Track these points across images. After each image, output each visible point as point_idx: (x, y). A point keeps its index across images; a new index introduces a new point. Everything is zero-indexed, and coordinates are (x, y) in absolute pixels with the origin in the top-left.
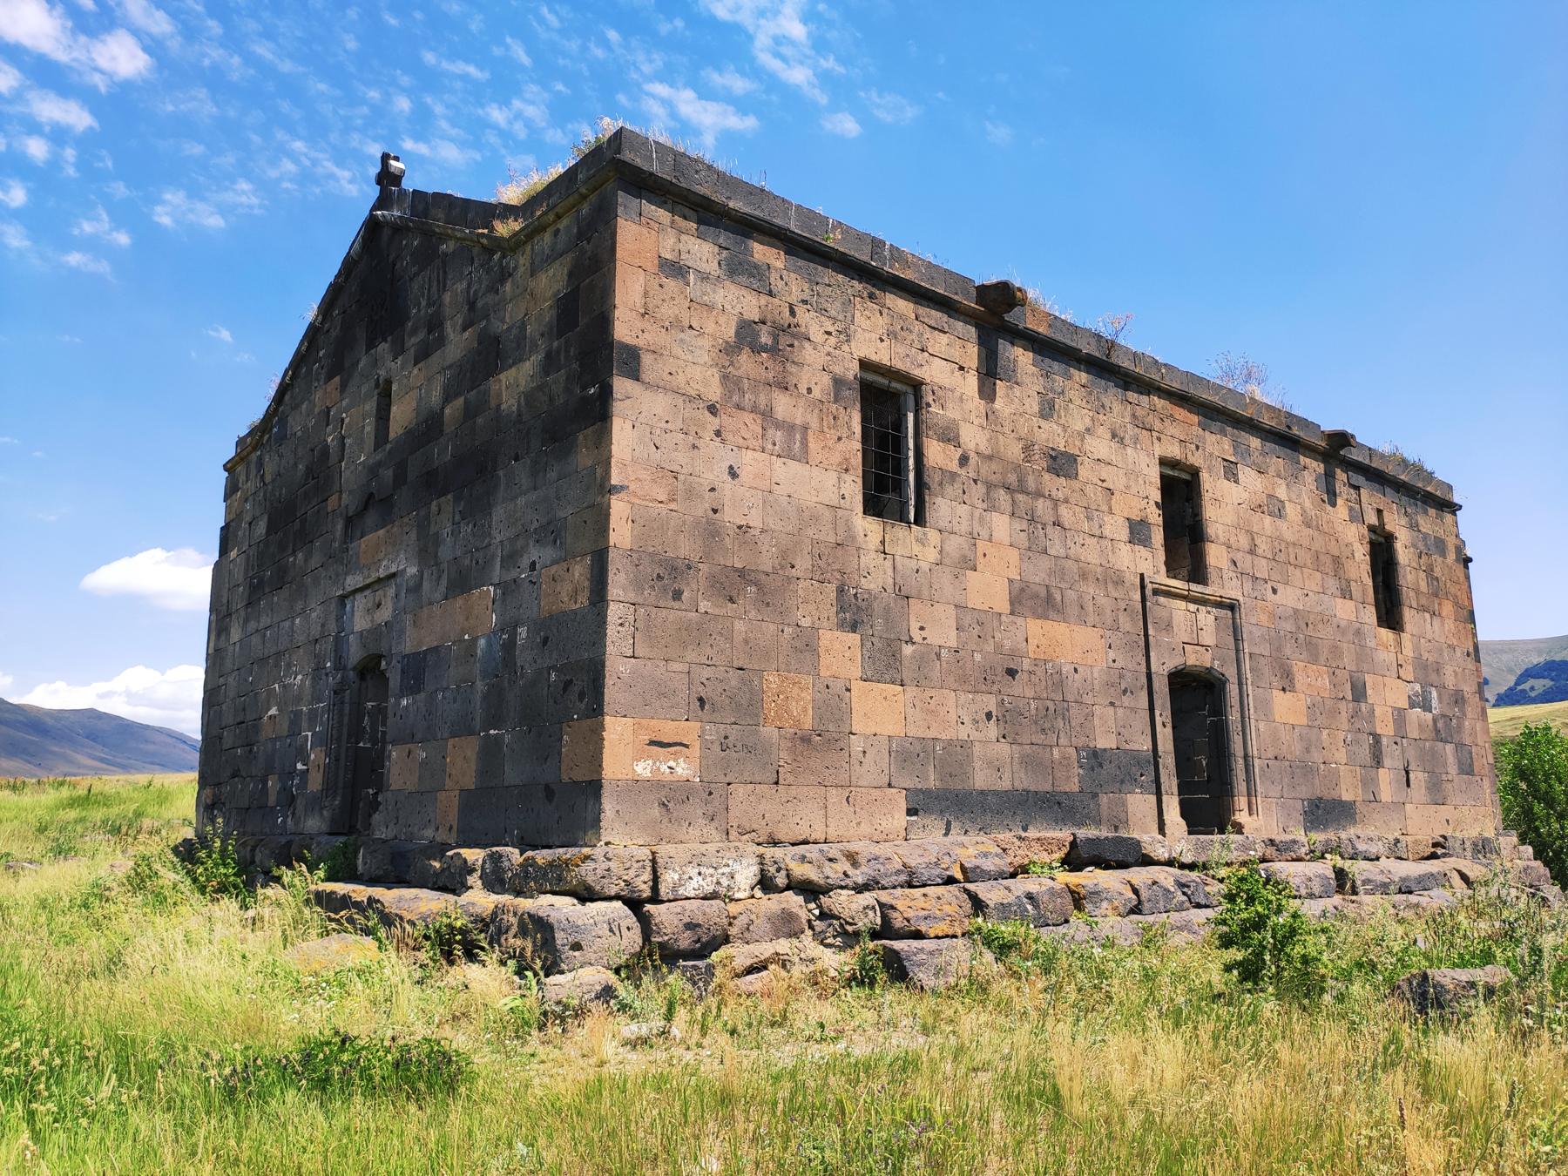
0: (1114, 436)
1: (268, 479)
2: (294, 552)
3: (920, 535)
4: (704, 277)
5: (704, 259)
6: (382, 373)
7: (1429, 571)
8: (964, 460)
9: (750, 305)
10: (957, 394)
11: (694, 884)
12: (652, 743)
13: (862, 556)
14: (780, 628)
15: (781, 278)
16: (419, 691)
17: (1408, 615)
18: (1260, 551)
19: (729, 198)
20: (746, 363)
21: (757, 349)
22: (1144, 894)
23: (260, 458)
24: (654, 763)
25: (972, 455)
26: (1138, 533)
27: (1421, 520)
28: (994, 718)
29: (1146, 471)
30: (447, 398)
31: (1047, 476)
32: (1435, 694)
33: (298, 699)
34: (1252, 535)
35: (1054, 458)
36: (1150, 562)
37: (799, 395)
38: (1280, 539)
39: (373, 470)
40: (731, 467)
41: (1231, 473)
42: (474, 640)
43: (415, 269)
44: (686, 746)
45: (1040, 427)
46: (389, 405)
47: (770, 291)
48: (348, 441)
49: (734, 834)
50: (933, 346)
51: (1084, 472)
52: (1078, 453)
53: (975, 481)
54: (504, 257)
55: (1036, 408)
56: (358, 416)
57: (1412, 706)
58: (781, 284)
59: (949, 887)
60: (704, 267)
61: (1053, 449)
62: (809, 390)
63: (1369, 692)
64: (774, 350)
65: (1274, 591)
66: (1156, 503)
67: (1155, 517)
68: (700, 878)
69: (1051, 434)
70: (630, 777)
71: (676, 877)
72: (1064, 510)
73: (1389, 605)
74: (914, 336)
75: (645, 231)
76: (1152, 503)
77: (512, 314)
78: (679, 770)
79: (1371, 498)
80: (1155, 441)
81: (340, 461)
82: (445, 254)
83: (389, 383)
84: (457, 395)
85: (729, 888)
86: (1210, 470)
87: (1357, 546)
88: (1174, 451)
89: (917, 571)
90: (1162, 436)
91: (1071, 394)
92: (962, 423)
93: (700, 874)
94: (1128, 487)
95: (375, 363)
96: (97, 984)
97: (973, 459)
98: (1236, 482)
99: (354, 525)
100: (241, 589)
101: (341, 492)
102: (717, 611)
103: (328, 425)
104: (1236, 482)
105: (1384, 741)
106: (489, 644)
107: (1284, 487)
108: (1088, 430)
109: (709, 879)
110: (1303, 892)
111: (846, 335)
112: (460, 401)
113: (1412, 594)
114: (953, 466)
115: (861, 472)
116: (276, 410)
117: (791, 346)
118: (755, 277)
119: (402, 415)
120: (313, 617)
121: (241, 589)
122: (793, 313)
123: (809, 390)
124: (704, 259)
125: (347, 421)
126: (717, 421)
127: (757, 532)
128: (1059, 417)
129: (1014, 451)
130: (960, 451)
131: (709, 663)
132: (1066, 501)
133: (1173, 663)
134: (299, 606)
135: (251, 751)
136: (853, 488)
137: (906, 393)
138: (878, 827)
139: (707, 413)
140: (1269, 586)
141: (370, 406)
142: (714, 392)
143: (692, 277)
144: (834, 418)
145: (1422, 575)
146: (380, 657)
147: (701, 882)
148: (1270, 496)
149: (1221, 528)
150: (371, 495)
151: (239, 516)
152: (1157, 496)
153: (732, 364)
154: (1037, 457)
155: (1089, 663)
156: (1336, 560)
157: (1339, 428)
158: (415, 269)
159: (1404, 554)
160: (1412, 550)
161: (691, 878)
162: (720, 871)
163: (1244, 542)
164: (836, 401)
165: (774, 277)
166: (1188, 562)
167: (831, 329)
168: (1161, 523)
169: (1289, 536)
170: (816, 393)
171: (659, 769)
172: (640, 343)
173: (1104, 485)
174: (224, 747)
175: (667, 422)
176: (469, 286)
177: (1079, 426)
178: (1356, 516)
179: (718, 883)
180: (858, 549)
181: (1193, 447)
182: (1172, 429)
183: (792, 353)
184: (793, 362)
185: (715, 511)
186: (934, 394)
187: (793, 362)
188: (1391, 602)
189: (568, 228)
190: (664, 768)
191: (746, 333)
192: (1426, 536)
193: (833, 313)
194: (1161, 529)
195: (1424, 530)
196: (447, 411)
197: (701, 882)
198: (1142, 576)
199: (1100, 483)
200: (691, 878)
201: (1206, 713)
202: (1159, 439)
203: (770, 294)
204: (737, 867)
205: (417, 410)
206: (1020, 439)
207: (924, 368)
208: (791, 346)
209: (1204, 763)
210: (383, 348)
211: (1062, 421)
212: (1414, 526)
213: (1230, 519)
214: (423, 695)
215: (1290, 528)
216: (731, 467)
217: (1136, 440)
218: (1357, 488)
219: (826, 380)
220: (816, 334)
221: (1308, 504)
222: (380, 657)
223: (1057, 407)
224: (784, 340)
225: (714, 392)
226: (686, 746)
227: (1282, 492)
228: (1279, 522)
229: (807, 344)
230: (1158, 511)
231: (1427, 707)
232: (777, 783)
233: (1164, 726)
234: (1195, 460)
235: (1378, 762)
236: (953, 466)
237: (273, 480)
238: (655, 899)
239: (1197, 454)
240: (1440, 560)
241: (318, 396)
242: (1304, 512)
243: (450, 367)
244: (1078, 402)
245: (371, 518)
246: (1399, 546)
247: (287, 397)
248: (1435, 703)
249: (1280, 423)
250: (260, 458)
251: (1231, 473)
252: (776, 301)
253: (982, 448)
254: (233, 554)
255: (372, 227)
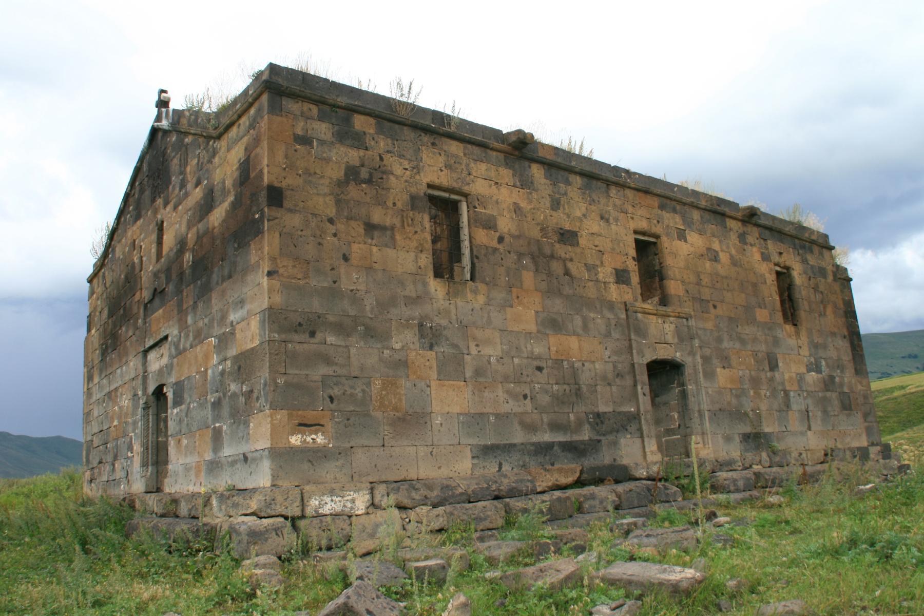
0: (602, 218)
1: (108, 285)
2: (121, 327)
3: (473, 288)
4: (322, 142)
5: (323, 132)
6: (159, 217)
7: (816, 289)
8: (501, 240)
9: (353, 156)
10: (494, 198)
11: (328, 506)
12: (300, 425)
13: (434, 303)
14: (381, 351)
15: (373, 139)
16: (181, 405)
17: (802, 314)
18: (704, 283)
19: (338, 96)
20: (353, 192)
21: (359, 181)
22: (623, 497)
23: (104, 273)
24: (302, 437)
25: (506, 236)
26: (621, 277)
27: (809, 257)
28: (529, 398)
29: (625, 238)
30: (189, 228)
31: (557, 246)
32: (823, 363)
33: (127, 414)
34: (698, 275)
35: (562, 234)
36: (630, 293)
37: (387, 208)
38: (717, 274)
39: (156, 275)
40: (344, 255)
41: (682, 236)
42: (206, 370)
43: (173, 154)
44: (322, 426)
45: (551, 216)
46: (163, 235)
47: (366, 147)
48: (144, 259)
49: (356, 478)
50: (476, 171)
51: (583, 241)
52: (578, 230)
53: (509, 252)
54: (214, 142)
55: (548, 205)
56: (148, 244)
57: (809, 371)
58: (373, 143)
59: (495, 502)
60: (323, 137)
61: (561, 229)
62: (394, 204)
63: (780, 364)
64: (369, 181)
65: (715, 307)
66: (633, 258)
67: (632, 266)
68: (333, 504)
69: (560, 219)
70: (287, 445)
71: (317, 503)
72: (569, 265)
73: (792, 311)
74: (463, 167)
75: (285, 119)
76: (630, 257)
77: (217, 176)
78: (319, 440)
79: (772, 247)
80: (630, 220)
81: (141, 271)
82: (188, 144)
83: (162, 222)
84: (194, 226)
85: (352, 508)
86: (668, 235)
87: (767, 275)
88: (643, 225)
89: (472, 310)
90: (634, 216)
91: (571, 194)
92: (498, 217)
93: (332, 500)
94: (613, 249)
95: (156, 212)
96: (380, 600)
97: (508, 239)
98: (686, 241)
99: (148, 307)
100: (98, 352)
101: (141, 289)
102: (339, 343)
103: (134, 250)
104: (686, 241)
105: (792, 394)
106: (213, 373)
107: (717, 242)
108: (584, 215)
109: (338, 503)
110: (732, 488)
111: (417, 169)
112: (195, 229)
113: (805, 302)
114: (494, 244)
115: (431, 251)
116: (110, 244)
117: (382, 178)
118: (358, 140)
119: (169, 239)
120: (133, 364)
121: (98, 352)
122: (381, 159)
123: (394, 204)
124: (323, 132)
125: (143, 247)
126: (334, 227)
127: (363, 293)
128: (564, 209)
129: (535, 233)
130: (498, 234)
131: (335, 374)
132: (571, 260)
133: (649, 357)
134: (124, 360)
135: (107, 447)
136: (426, 260)
137: (460, 201)
138: (452, 468)
139: (328, 224)
140: (711, 305)
141: (154, 237)
142: (331, 212)
143: (315, 143)
144: (412, 220)
145: (812, 291)
146: (163, 385)
147: (333, 506)
148: (709, 249)
149: (677, 270)
150: (155, 290)
151: (95, 308)
152: (633, 252)
153: (342, 193)
154: (550, 234)
155: (593, 359)
156: (755, 285)
157: (750, 204)
158: (173, 154)
159: (798, 277)
160: (804, 276)
161: (326, 503)
162: (345, 498)
163: (692, 278)
164: (412, 209)
165: (368, 139)
166: (659, 292)
167: (407, 167)
168: (637, 270)
169: (722, 271)
170: (399, 205)
171: (305, 440)
172: (284, 185)
173: (597, 249)
174: (95, 446)
175: (302, 230)
176: (199, 161)
177: (578, 214)
178: (765, 258)
179: (344, 506)
180: (431, 299)
181: (655, 222)
182: (641, 212)
183: (382, 182)
184: (383, 188)
185: (335, 282)
186: (478, 200)
187: (383, 188)
188: (794, 309)
189: (244, 123)
190: (309, 439)
191: (352, 174)
192: (812, 267)
193: (409, 157)
194: (637, 274)
195: (811, 263)
196: (189, 235)
197: (333, 506)
198: (625, 303)
199: (594, 247)
200: (326, 503)
201: (675, 385)
202: (632, 218)
203: (367, 149)
204: (356, 495)
205: (175, 237)
206: (538, 224)
207: (471, 185)
208: (382, 178)
209: (676, 417)
210: (159, 201)
211: (567, 211)
212: (804, 261)
213: (682, 264)
214: (183, 407)
215: (724, 266)
216: (344, 255)
217: (616, 220)
218: (765, 240)
219: (406, 197)
220: (398, 171)
221: (733, 252)
222: (163, 385)
223: (562, 202)
224: (377, 175)
225: (331, 212)
226: (322, 426)
227: (716, 246)
228: (715, 264)
229: (391, 177)
230: (634, 263)
231: (818, 370)
232: (383, 446)
233: (644, 395)
234: (657, 230)
235: (788, 407)
236: (494, 244)
237: (110, 286)
238: (303, 517)
239: (659, 226)
240: (823, 280)
241: (129, 233)
242: (732, 257)
243: (190, 209)
244: (577, 199)
245: (157, 301)
246: (795, 274)
247: (115, 236)
248: (823, 369)
249: (712, 205)
250: (104, 273)
251: (682, 236)
252: (370, 153)
253: (513, 231)
254: (93, 331)
255: (154, 132)
